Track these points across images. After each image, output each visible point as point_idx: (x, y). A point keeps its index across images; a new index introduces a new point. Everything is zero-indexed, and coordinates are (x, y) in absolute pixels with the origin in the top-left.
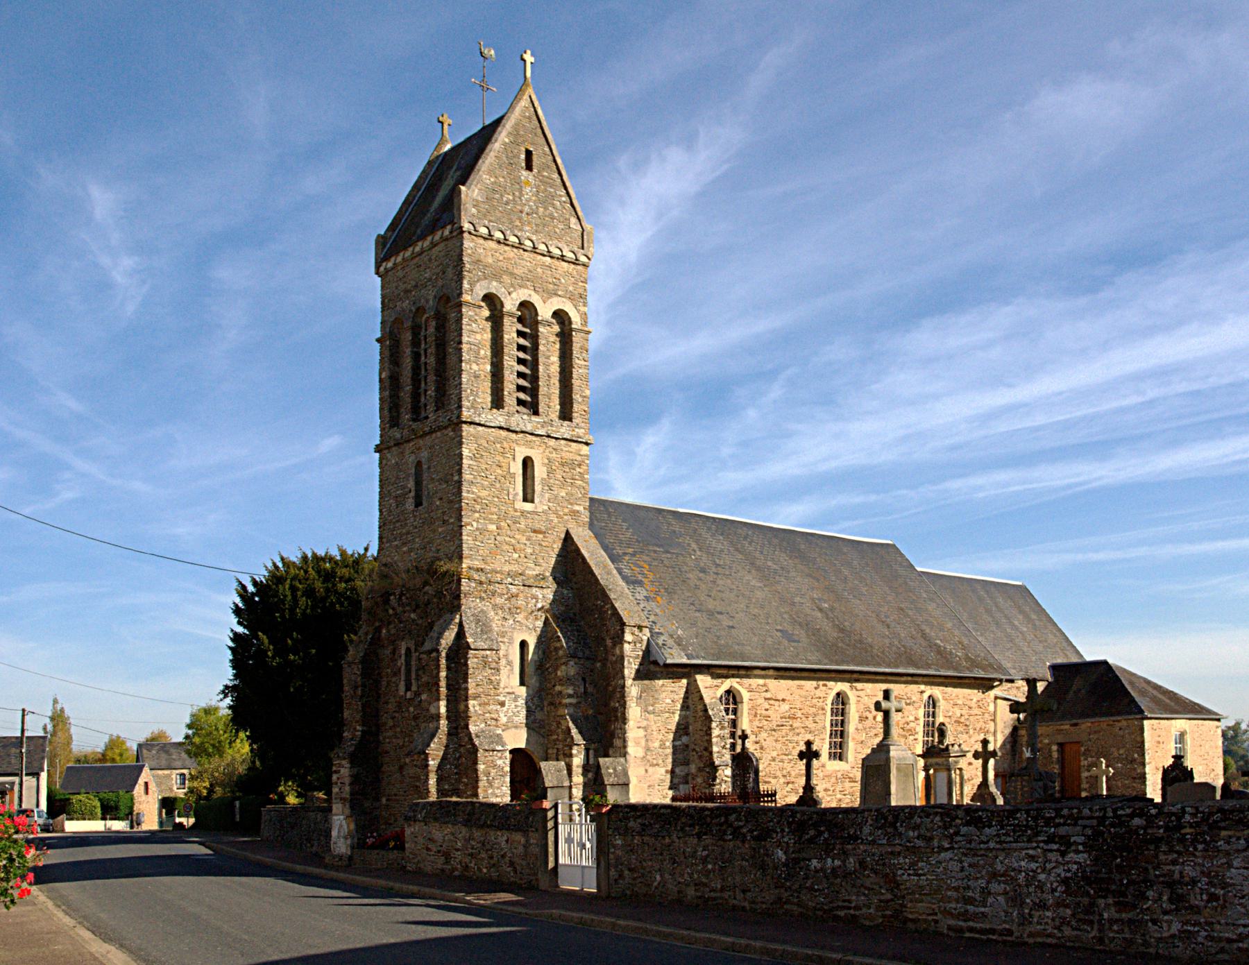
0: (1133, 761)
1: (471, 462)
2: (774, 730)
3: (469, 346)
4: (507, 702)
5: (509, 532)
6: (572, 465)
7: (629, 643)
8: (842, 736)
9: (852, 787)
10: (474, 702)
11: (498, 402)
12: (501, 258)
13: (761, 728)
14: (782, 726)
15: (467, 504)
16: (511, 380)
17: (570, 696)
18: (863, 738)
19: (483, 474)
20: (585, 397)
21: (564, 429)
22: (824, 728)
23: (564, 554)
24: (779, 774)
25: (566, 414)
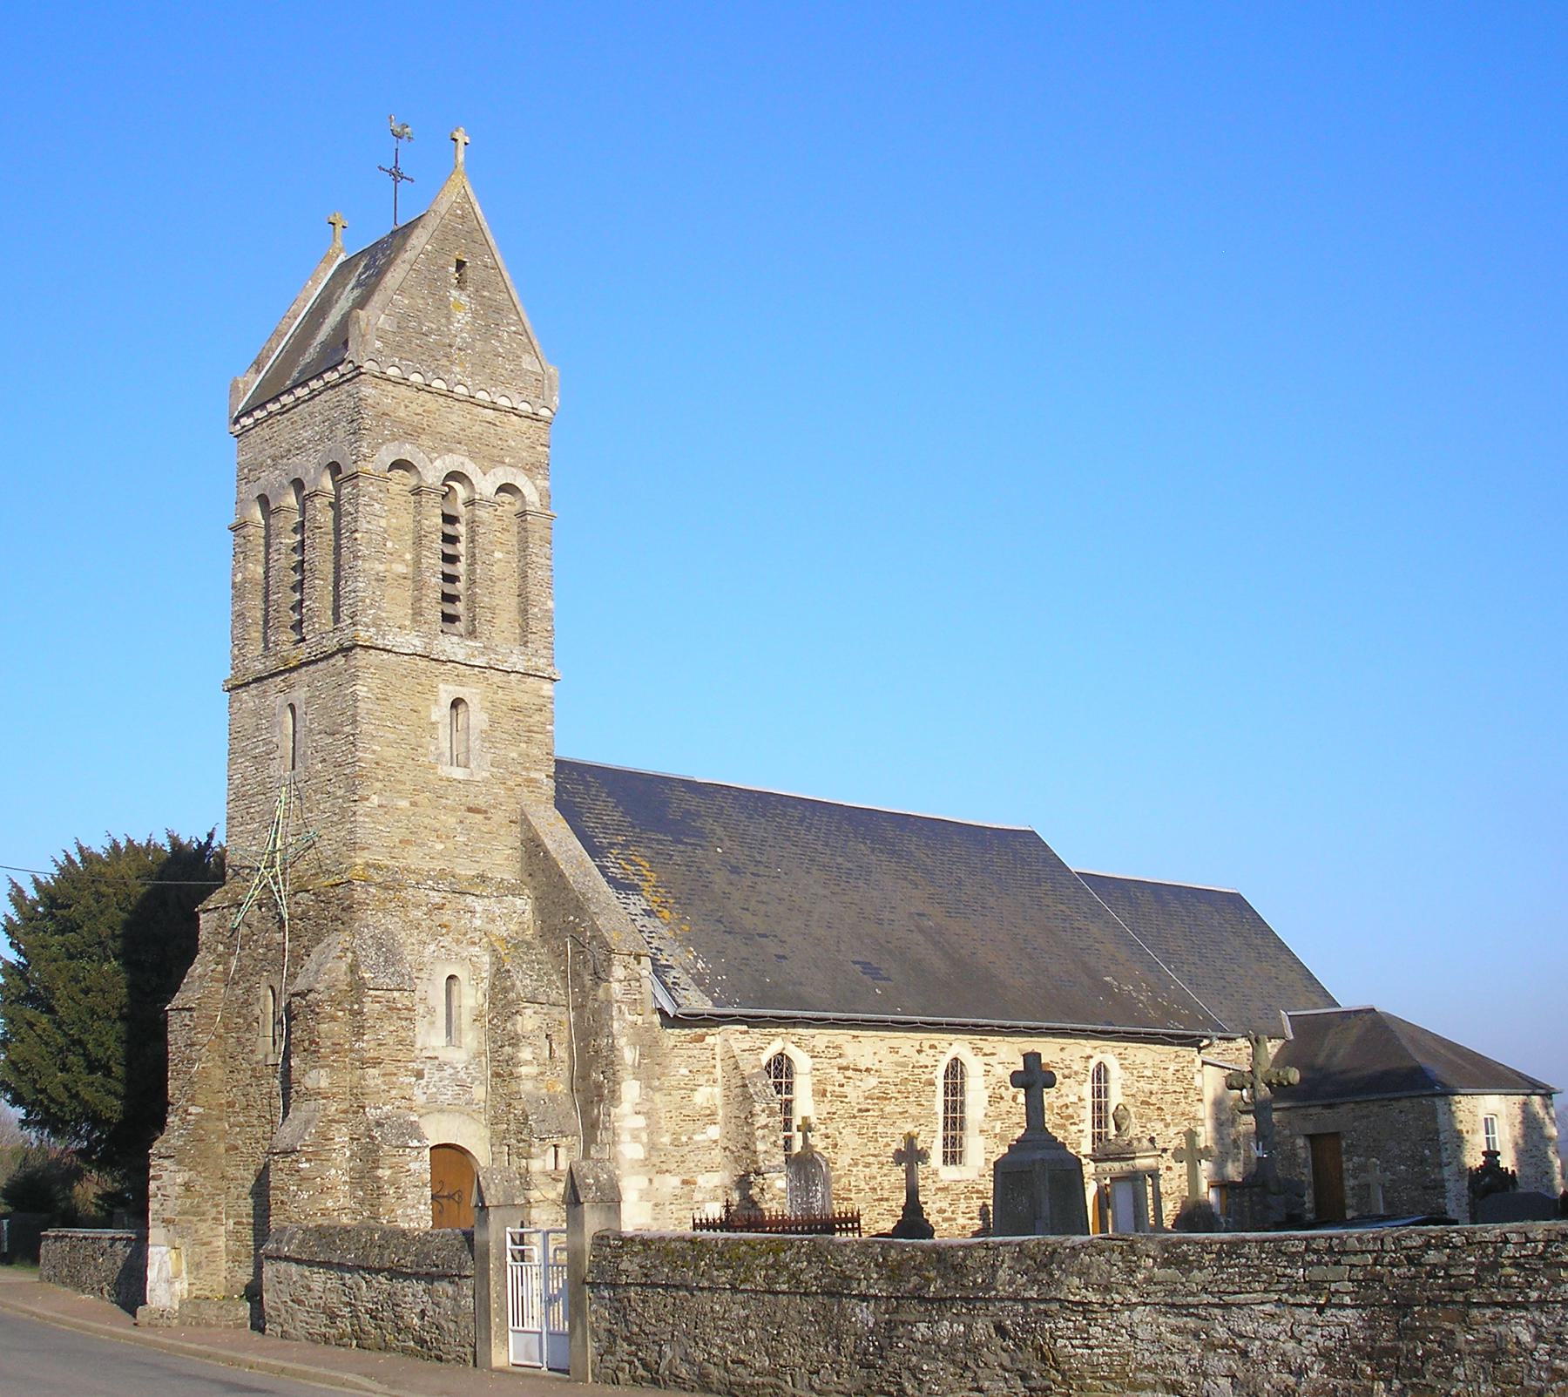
14: (868, 1110)
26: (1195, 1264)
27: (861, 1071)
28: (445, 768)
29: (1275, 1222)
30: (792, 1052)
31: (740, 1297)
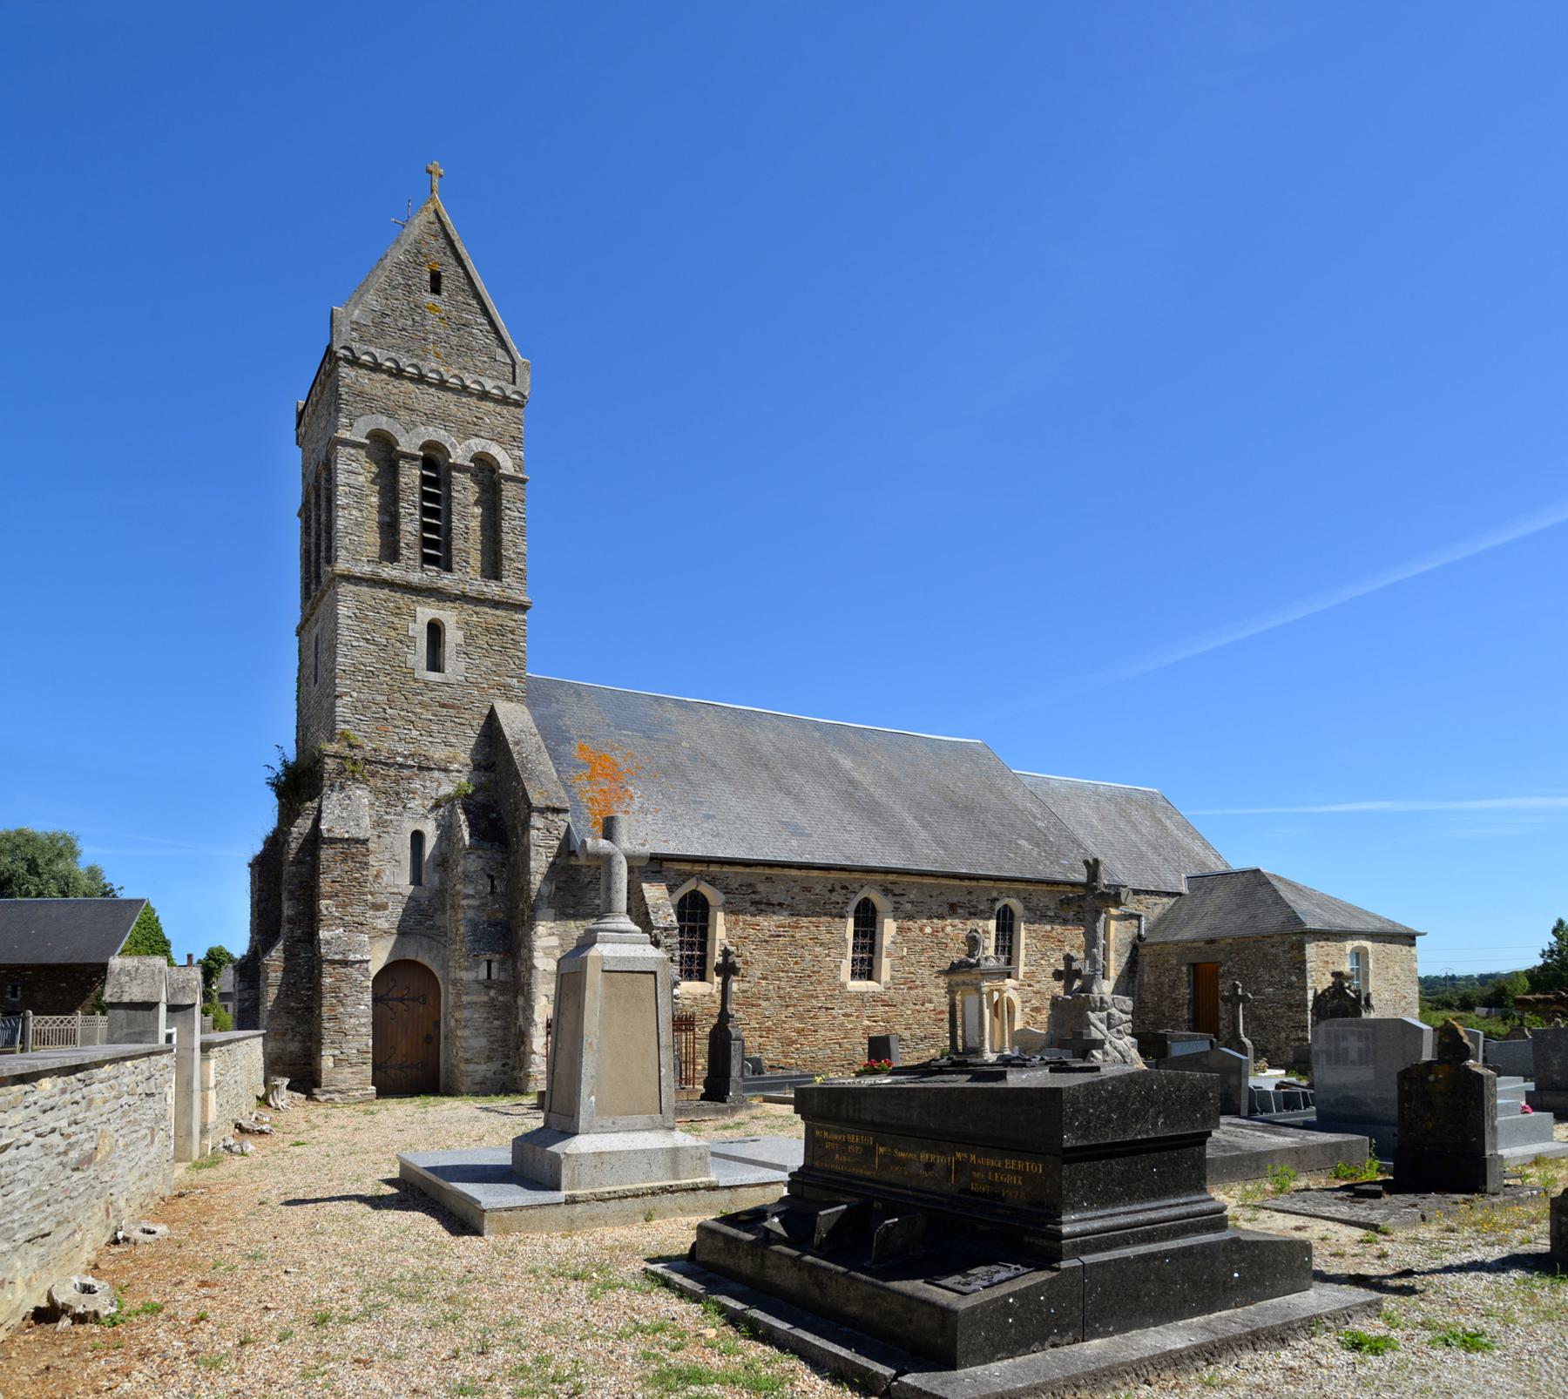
0: (1290, 985)
1: (350, 622)
2: (766, 941)
3: (347, 489)
4: (390, 904)
5: (406, 706)
6: (501, 631)
7: (538, 829)
8: (872, 951)
9: (886, 1012)
10: (328, 902)
11: (391, 553)
12: (394, 391)
13: (745, 938)
14: (780, 936)
15: (344, 671)
16: (410, 527)
17: (467, 897)
18: (905, 954)
19: (368, 637)
20: (519, 553)
21: (493, 589)
22: (845, 940)
23: (488, 733)
24: (773, 994)
25: (493, 568)
26: (1405, 966)
27: (773, 905)
28: (421, 672)
29: (478, 1232)
30: (705, 889)
31: (80, 1201)
